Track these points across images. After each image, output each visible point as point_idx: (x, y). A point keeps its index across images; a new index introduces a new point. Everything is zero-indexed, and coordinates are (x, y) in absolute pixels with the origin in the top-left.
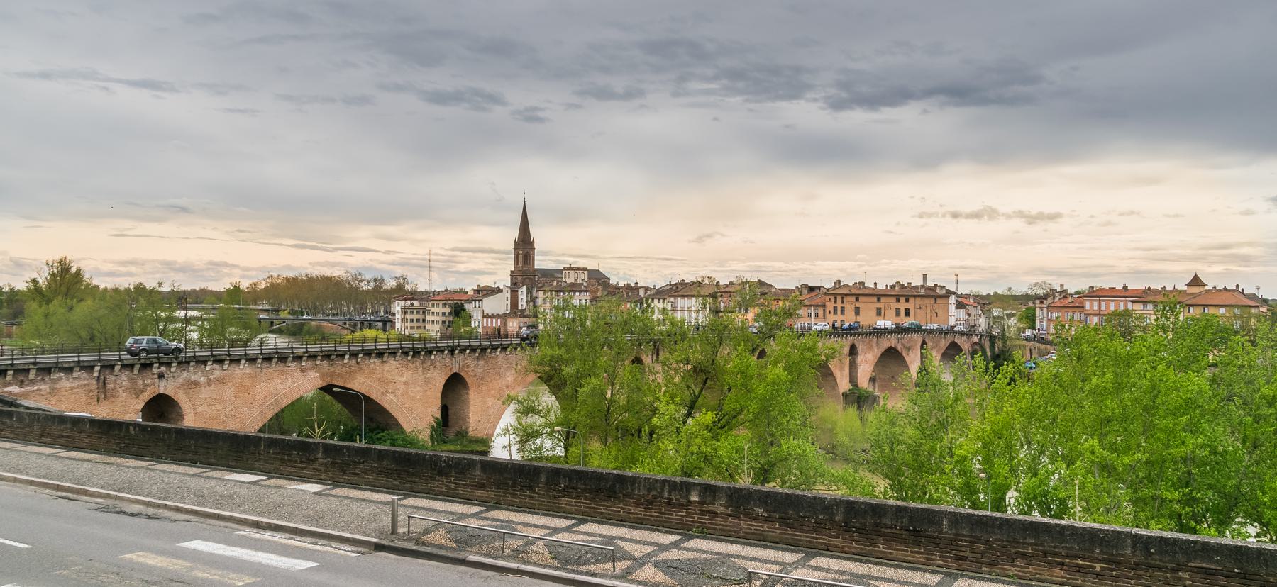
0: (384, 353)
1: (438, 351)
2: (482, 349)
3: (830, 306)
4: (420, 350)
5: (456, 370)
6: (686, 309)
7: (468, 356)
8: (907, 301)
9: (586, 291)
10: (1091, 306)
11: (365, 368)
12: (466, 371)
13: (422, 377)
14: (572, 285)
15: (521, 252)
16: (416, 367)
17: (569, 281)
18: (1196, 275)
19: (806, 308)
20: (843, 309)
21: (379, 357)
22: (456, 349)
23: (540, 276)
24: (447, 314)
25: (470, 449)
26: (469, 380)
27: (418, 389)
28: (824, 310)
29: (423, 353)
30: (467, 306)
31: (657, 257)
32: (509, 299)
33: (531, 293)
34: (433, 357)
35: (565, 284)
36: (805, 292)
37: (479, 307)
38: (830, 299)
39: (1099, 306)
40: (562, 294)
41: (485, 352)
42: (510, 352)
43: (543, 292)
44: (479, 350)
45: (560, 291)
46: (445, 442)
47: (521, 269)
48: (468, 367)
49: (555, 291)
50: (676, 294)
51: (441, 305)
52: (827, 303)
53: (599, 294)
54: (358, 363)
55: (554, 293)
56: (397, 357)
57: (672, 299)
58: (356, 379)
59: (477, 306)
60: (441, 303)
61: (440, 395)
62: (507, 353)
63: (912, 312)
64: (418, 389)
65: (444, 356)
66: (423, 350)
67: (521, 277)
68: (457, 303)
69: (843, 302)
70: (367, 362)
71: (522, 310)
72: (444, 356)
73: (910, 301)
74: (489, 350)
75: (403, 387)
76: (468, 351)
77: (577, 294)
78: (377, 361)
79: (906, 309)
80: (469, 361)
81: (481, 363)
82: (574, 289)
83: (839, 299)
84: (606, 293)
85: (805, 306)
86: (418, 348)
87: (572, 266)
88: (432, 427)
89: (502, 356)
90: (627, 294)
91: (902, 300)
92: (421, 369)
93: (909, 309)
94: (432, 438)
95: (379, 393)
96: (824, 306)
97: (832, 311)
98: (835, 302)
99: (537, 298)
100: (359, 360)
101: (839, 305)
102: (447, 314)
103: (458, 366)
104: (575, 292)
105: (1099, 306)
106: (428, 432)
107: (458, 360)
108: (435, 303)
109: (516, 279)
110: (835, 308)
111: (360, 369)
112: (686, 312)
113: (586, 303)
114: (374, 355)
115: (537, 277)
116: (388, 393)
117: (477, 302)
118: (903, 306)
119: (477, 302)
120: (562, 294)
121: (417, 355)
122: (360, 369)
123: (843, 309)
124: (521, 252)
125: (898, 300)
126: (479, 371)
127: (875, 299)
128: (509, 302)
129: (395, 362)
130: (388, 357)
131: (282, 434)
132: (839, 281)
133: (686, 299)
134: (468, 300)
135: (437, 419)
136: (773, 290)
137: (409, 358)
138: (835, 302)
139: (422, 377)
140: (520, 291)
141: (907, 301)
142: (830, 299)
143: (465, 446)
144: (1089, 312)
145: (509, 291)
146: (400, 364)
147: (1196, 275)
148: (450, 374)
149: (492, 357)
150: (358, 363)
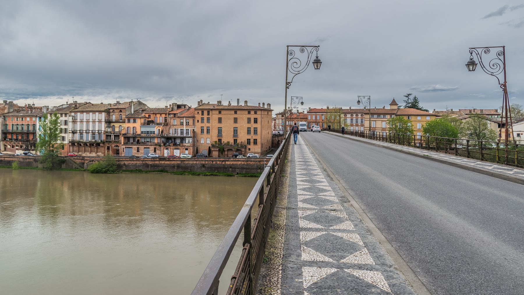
3: (198, 117)
6: (85, 120)
8: (255, 113)
10: (312, 117)
18: (394, 99)
19: (179, 119)
20: (208, 119)
28: (194, 120)
36: (176, 108)
38: (198, 113)
39: (316, 117)
50: (76, 110)
52: (196, 115)
57: (73, 114)
63: (259, 121)
69: (208, 114)
73: (258, 113)
79: (255, 119)
83: (206, 112)
85: (179, 117)
91: (252, 112)
93: (257, 118)
96: (194, 117)
97: (200, 121)
98: (203, 114)
101: (205, 116)
105: (316, 117)
110: (202, 119)
112: (85, 124)
118: (252, 116)
123: (208, 119)
125: (249, 113)
127: (247, 112)
132: (202, 101)
133: (85, 114)
136: (146, 108)
138: (203, 114)
141: (255, 113)
142: (198, 113)
144: (311, 121)
147: (394, 99)
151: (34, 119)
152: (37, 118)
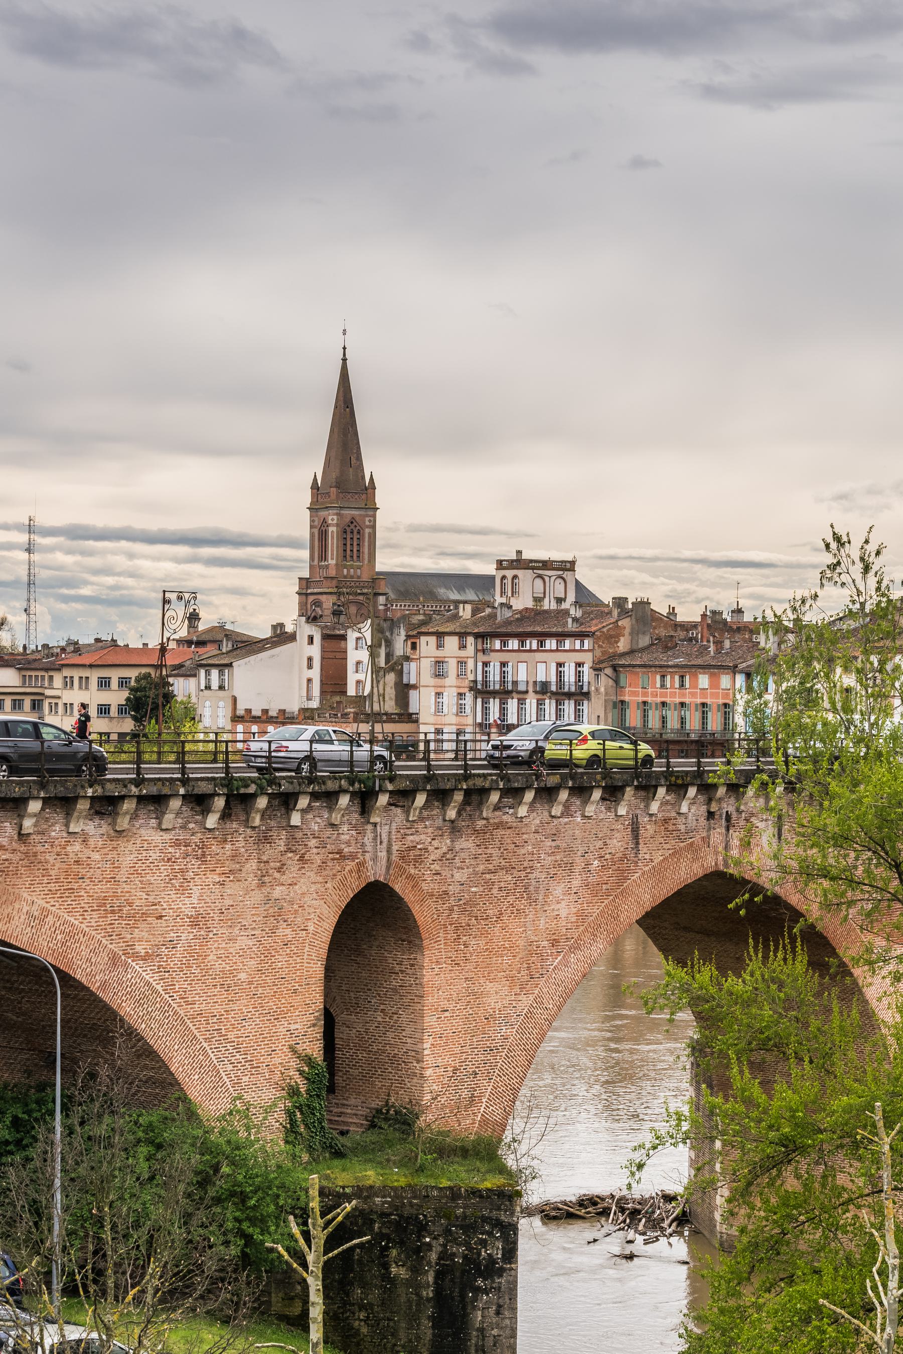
0: (122, 798)
1: (315, 796)
2: (468, 793)
4: (252, 789)
5: (376, 872)
7: (422, 819)
9: (582, 635)
11: (51, 858)
12: (410, 877)
13: (257, 896)
14: (526, 615)
15: (332, 519)
16: (234, 857)
17: (519, 604)
21: (99, 813)
22: (382, 790)
23: (392, 596)
24: (114, 711)
25: (445, 1183)
26: (422, 913)
27: (244, 942)
29: (262, 802)
30: (181, 687)
31: (687, 554)
32: (317, 663)
33: (389, 644)
34: (296, 819)
35: (508, 614)
37: (221, 688)
40: (497, 644)
41: (481, 804)
42: (567, 806)
43: (432, 640)
44: (459, 797)
45: (494, 635)
46: (338, 1154)
47: (332, 572)
48: (418, 861)
49: (477, 636)
51: (94, 683)
53: (623, 645)
54: (22, 837)
55: (470, 640)
56: (169, 819)
58: (18, 898)
59: (215, 684)
60: (94, 676)
61: (317, 969)
62: (557, 810)
64: (244, 942)
65: (336, 817)
66: (262, 791)
67: (332, 599)
68: (147, 676)
70: (57, 831)
71: (360, 700)
72: (336, 817)
74: (495, 797)
75: (186, 935)
76: (421, 799)
77: (551, 644)
78: (94, 829)
80: (423, 836)
81: (466, 844)
82: (539, 629)
84: (644, 641)
86: (246, 782)
87: (526, 556)
88: (293, 1092)
89: (535, 820)
90: (719, 644)
92: (253, 865)
94: (291, 1130)
95: (103, 959)
99: (407, 659)
100: (28, 824)
102: (114, 711)
103: (383, 855)
104: (542, 636)
106: (278, 1118)
107: (384, 831)
108: (76, 674)
109: (318, 604)
111: (32, 860)
113: (579, 675)
114: (83, 806)
115: (382, 600)
116: (136, 956)
117: (215, 673)
119: (215, 673)
120: (497, 644)
121: (238, 809)
122: (32, 860)
124: (332, 519)
126: (458, 876)
128: (315, 674)
129: (158, 837)
130: (134, 816)
131: (63, 1105)
134: (181, 666)
135: (309, 1060)
137: (212, 821)
139: (257, 896)
140: (352, 636)
143: (421, 1169)
145: (317, 639)
146: (177, 844)
148: (355, 886)
149: (501, 825)
150: (22, 837)
151: (725, 681)
152: (740, 680)
